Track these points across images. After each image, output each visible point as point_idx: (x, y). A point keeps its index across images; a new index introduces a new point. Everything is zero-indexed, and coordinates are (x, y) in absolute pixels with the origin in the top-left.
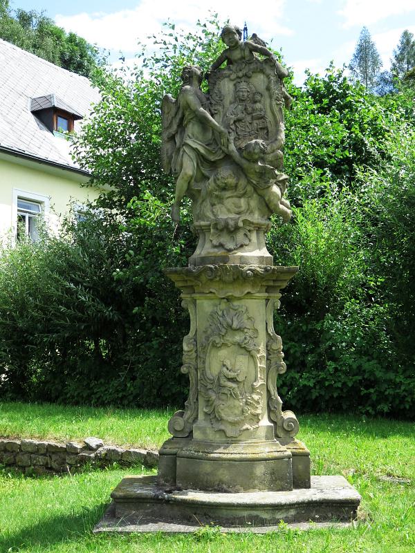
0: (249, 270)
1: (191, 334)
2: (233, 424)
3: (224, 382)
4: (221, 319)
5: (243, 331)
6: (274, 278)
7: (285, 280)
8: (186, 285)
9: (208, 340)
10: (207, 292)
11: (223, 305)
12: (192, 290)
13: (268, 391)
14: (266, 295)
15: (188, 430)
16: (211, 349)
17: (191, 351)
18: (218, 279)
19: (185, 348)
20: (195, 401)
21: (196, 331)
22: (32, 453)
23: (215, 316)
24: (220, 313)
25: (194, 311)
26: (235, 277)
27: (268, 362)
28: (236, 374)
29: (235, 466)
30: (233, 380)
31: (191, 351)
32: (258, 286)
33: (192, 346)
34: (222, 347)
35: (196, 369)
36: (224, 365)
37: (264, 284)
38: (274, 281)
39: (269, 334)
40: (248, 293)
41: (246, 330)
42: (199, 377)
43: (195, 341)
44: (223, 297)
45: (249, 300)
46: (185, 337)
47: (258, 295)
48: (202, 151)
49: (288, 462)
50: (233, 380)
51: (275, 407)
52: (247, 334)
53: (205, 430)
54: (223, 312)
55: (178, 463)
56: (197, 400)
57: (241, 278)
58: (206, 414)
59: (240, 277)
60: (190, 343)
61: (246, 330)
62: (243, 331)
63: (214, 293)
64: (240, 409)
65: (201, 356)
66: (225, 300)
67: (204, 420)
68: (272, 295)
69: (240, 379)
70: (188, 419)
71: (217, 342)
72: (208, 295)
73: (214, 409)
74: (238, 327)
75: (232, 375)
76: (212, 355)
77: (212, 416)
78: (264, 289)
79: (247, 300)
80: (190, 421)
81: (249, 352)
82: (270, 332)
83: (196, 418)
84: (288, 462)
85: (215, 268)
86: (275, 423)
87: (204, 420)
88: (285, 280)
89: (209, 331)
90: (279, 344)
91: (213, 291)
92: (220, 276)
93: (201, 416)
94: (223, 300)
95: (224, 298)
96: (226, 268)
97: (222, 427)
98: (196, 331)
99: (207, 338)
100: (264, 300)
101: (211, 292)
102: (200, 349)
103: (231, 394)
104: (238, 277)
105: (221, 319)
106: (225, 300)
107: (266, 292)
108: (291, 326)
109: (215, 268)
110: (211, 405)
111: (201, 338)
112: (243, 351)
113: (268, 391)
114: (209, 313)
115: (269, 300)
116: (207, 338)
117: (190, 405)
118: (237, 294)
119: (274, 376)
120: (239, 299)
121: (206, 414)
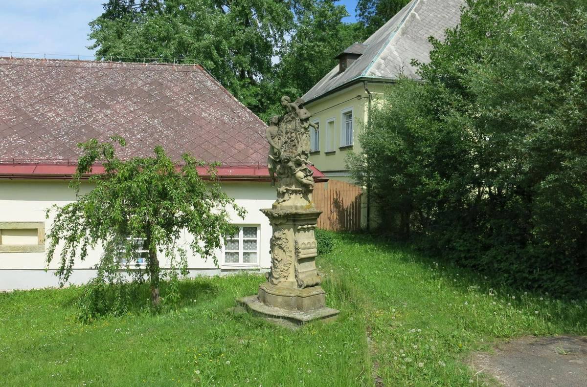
48: (272, 158)
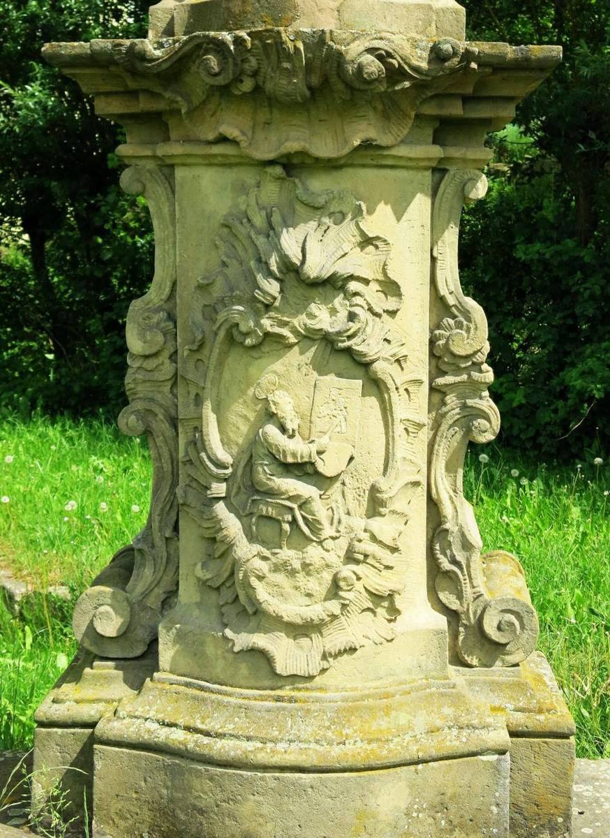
0: (371, 51)
1: (155, 293)
2: (302, 630)
3: (266, 474)
4: (261, 241)
5: (342, 288)
6: (469, 90)
7: (509, 99)
8: (133, 110)
9: (214, 321)
10: (211, 137)
11: (271, 192)
12: (157, 123)
13: (433, 504)
14: (436, 151)
15: (142, 634)
16: (223, 356)
17: (156, 355)
18: (247, 85)
19: (134, 342)
20: (168, 534)
21: (174, 284)
22: (279, 58)
23: (242, 230)
24: (259, 220)
25: (166, 210)
26: (315, 80)
27: (437, 398)
28: (314, 448)
29: (302, 790)
30: (304, 470)
31: (156, 355)
32: (406, 116)
33: (160, 338)
34: (265, 349)
35: (174, 422)
36: (271, 416)
37: (430, 110)
38: (466, 100)
39: (442, 299)
40: (367, 145)
41: (353, 286)
42: (181, 454)
43: (171, 317)
44: (271, 156)
45: (371, 174)
46: (136, 305)
47: (403, 151)
49: (496, 768)
50: (304, 470)
51: (454, 562)
52: (357, 300)
53: (202, 644)
54: (269, 216)
55: (98, 764)
56: (176, 528)
57: (340, 86)
58: (204, 585)
59: (334, 79)
60: (151, 328)
61: (353, 286)
62: (342, 288)
63: (234, 142)
64: (327, 577)
65: (190, 376)
66: (278, 170)
67: (199, 605)
68: (455, 152)
69: (327, 467)
70: (146, 595)
71: (243, 328)
72: (216, 150)
73: (232, 574)
74: (326, 274)
75: (296, 448)
76: (227, 375)
77: (227, 595)
78: (429, 132)
79: (363, 173)
80: (154, 601)
81: (367, 365)
82: (443, 291)
83: (173, 593)
84: (496, 768)
85: (238, 41)
86: (453, 616)
87: (199, 605)
88: (509, 99)
89: (218, 290)
90: (474, 335)
91: (232, 132)
92: (255, 74)
93: (188, 593)
94: (270, 170)
95: (271, 163)
96: (279, 43)
97: (260, 640)
98: (174, 284)
99: (211, 311)
100: (428, 174)
101: (222, 139)
102: (184, 352)
103: (294, 522)
104: (326, 80)
105: (261, 241)
106: (278, 170)
107: (435, 142)
108: (547, 401)
109: (238, 41)
110: (224, 555)
111: (190, 308)
112: (344, 362)
113: (433, 504)
114: (219, 218)
115: (445, 171)
116: (211, 311)
117: (153, 546)
118: (324, 148)
119: (450, 442)
120: (332, 165)
121: (204, 585)
